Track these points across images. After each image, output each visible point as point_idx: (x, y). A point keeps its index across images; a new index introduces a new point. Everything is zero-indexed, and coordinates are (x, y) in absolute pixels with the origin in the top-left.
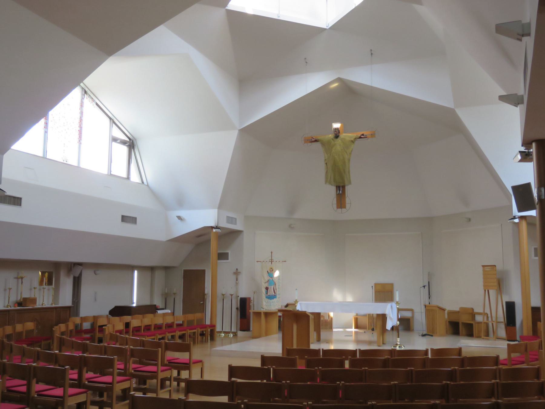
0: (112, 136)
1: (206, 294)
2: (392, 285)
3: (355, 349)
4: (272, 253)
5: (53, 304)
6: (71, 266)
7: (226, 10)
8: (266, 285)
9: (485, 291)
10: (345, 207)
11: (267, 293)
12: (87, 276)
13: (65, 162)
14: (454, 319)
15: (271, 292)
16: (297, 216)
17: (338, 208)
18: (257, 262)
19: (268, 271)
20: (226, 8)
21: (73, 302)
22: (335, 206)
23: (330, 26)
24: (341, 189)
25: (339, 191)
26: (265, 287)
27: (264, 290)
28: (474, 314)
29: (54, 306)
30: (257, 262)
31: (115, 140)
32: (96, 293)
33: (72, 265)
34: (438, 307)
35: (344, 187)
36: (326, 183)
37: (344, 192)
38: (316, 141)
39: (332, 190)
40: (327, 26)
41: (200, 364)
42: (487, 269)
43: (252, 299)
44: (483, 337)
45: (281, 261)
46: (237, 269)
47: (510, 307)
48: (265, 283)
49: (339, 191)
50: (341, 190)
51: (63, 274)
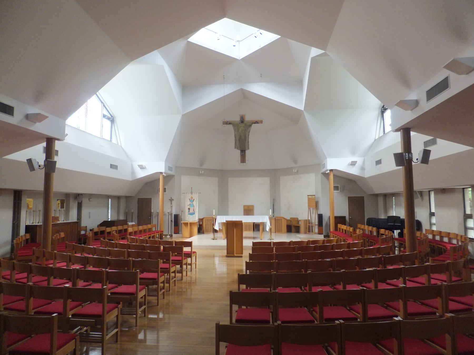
0: (103, 114)
1: (152, 213)
2: (253, 206)
3: (191, 241)
4: (192, 188)
5: (65, 221)
6: (77, 196)
7: (188, 41)
8: (189, 207)
9: (309, 208)
10: (245, 162)
11: (189, 212)
12: (85, 201)
13: (78, 128)
14: (289, 224)
15: (191, 211)
16: (204, 167)
17: (241, 163)
18: (183, 193)
19: (189, 199)
20: (188, 40)
21: (78, 219)
22: (240, 161)
23: (241, 58)
24: (244, 152)
25: (243, 153)
26: (188, 208)
27: (187, 210)
28: (299, 221)
29: (65, 222)
30: (183, 193)
31: (104, 116)
32: (90, 213)
33: (77, 195)
34: (283, 218)
35: (245, 151)
36: (235, 148)
37: (245, 153)
38: (230, 124)
39: (238, 152)
40: (239, 58)
41: (195, 253)
42: (310, 197)
43: (180, 215)
44: (307, 233)
45: (186, 193)
46: (171, 198)
47: (320, 217)
48: (188, 206)
49: (243, 153)
50: (243, 152)
51: (71, 200)
